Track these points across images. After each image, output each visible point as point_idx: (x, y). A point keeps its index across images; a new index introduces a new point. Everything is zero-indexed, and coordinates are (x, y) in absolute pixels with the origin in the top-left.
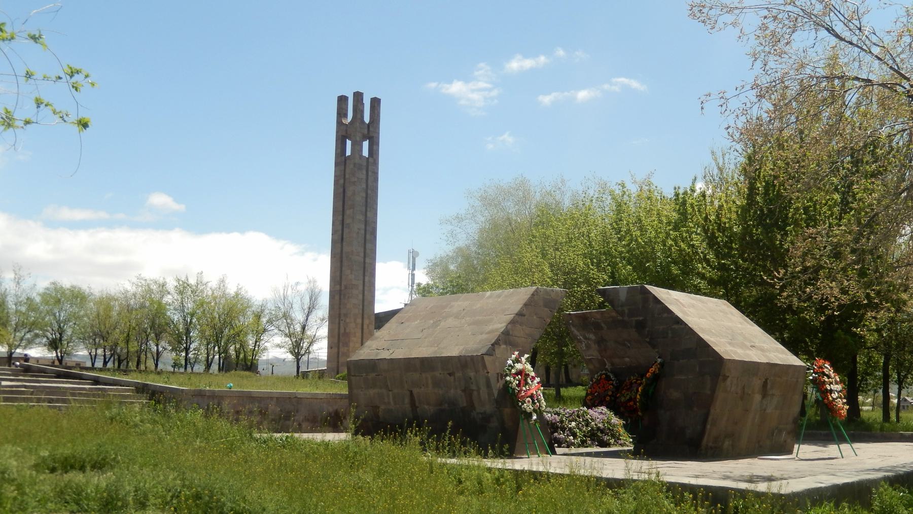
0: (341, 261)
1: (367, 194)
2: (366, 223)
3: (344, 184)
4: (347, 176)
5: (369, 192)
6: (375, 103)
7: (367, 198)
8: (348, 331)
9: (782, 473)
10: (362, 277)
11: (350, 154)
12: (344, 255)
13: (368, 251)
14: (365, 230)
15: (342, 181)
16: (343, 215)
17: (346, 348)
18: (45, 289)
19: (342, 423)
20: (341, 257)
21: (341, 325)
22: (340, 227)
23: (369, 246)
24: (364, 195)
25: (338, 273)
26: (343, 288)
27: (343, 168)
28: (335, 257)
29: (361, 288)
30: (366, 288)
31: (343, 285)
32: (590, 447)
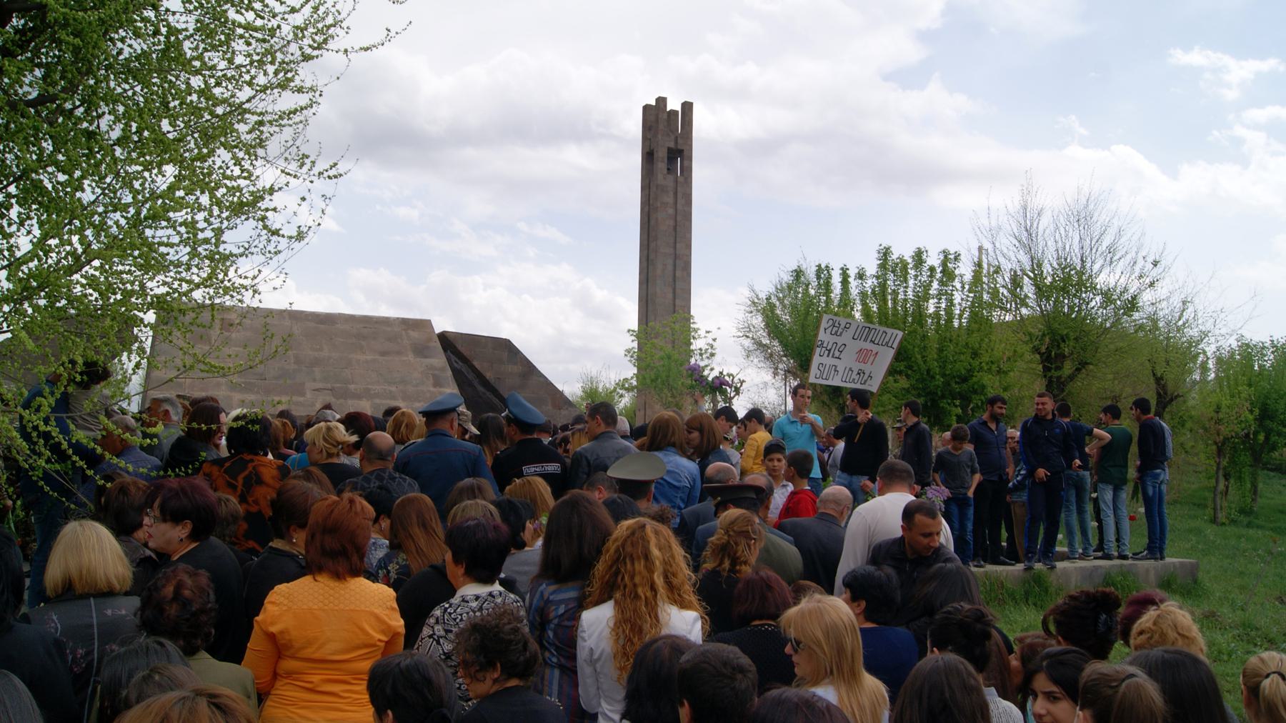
0: (647, 304)
1: (676, 221)
2: (676, 257)
3: (649, 212)
4: (651, 202)
5: (679, 218)
6: (687, 107)
7: (675, 228)
9: (788, 393)
14: (675, 266)
16: (648, 249)
18: (232, 516)
19: (1126, 290)
20: (647, 301)
23: (679, 285)
24: (672, 223)
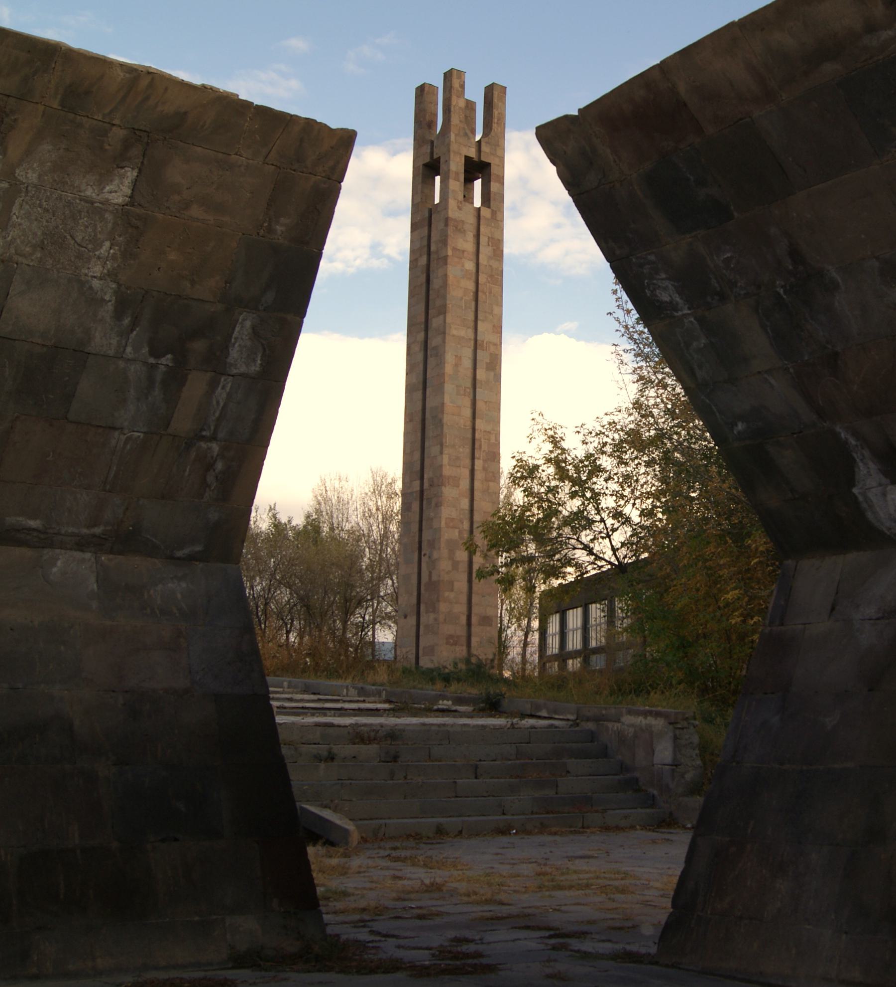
8: (434, 578)
10: (468, 462)
11: (436, 177)
12: (428, 415)
13: (480, 405)
15: (423, 260)
16: (426, 330)
17: (432, 616)
21: (424, 565)
22: (420, 356)
24: (471, 286)
25: (417, 455)
26: (426, 485)
27: (425, 231)
28: (411, 420)
29: (465, 484)
30: (477, 484)
31: (425, 481)
32: (358, 744)
